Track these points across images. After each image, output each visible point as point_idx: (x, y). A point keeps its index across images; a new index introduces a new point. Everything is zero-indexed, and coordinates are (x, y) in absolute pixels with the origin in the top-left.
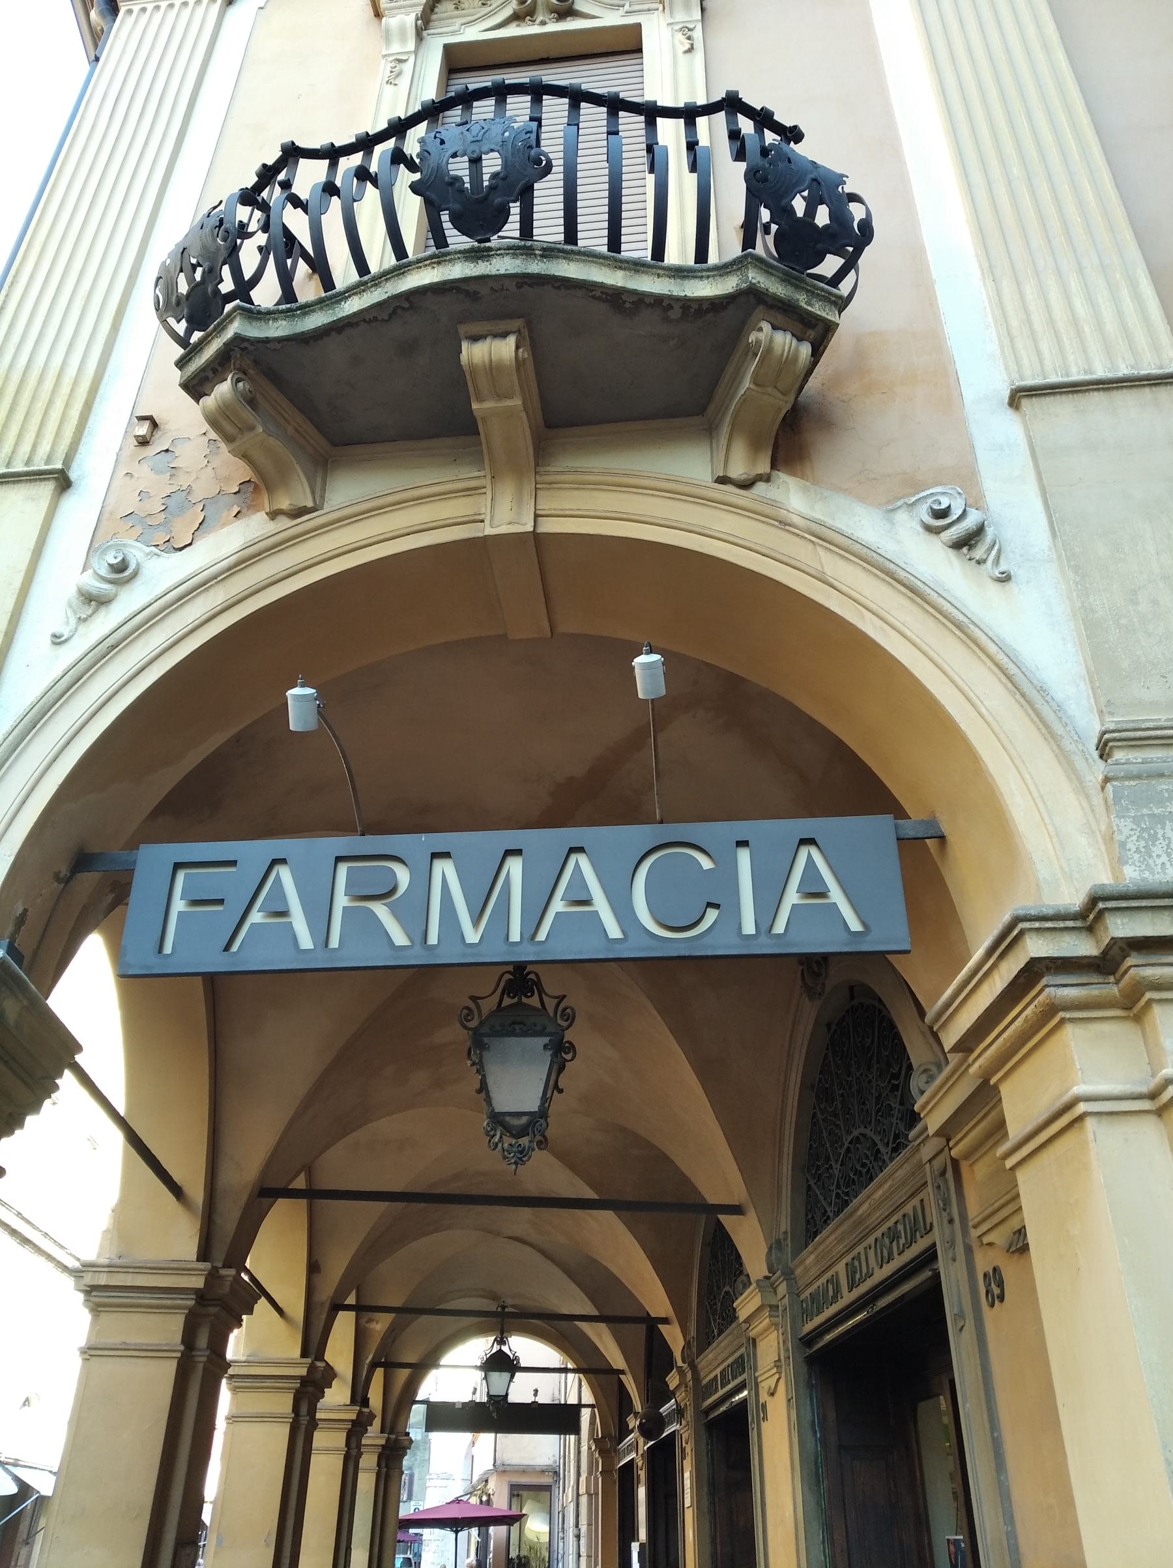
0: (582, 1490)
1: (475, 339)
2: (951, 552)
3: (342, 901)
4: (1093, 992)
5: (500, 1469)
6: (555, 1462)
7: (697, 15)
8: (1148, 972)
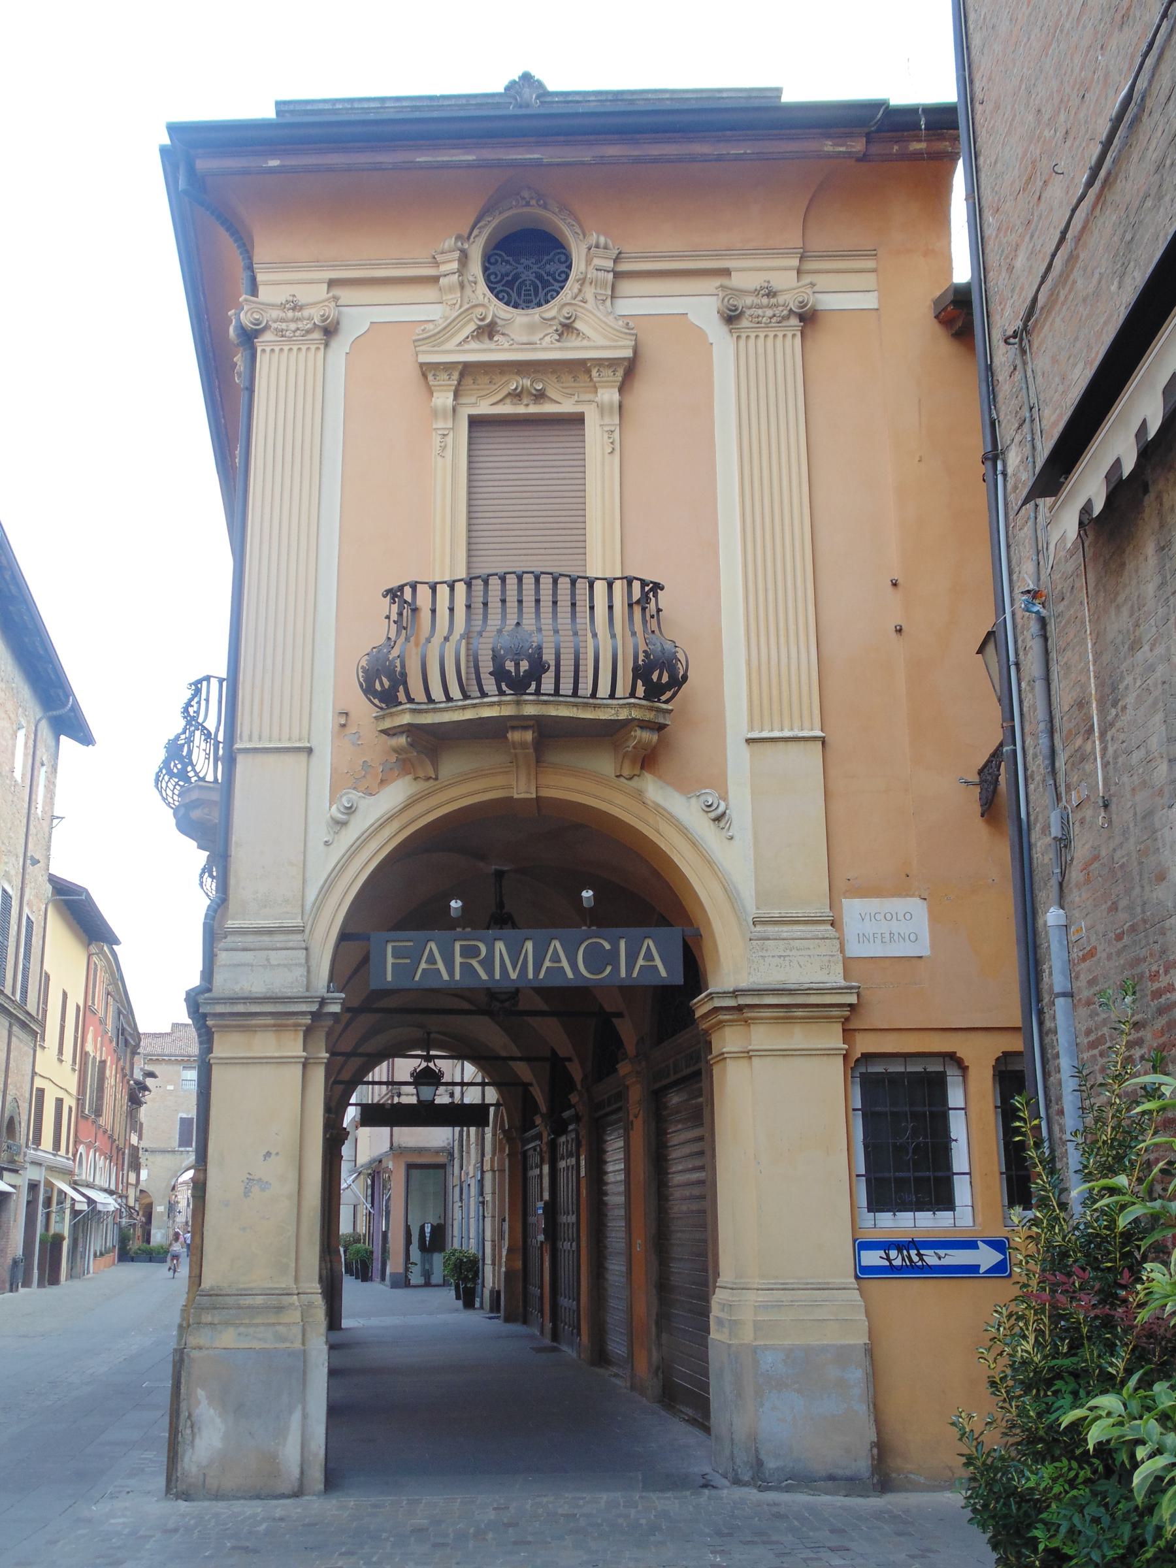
0: (487, 1167)
2: (712, 822)
3: (458, 960)
4: (735, 1017)
5: (396, 1150)
6: (449, 1144)
7: (617, 421)
8: (749, 1015)
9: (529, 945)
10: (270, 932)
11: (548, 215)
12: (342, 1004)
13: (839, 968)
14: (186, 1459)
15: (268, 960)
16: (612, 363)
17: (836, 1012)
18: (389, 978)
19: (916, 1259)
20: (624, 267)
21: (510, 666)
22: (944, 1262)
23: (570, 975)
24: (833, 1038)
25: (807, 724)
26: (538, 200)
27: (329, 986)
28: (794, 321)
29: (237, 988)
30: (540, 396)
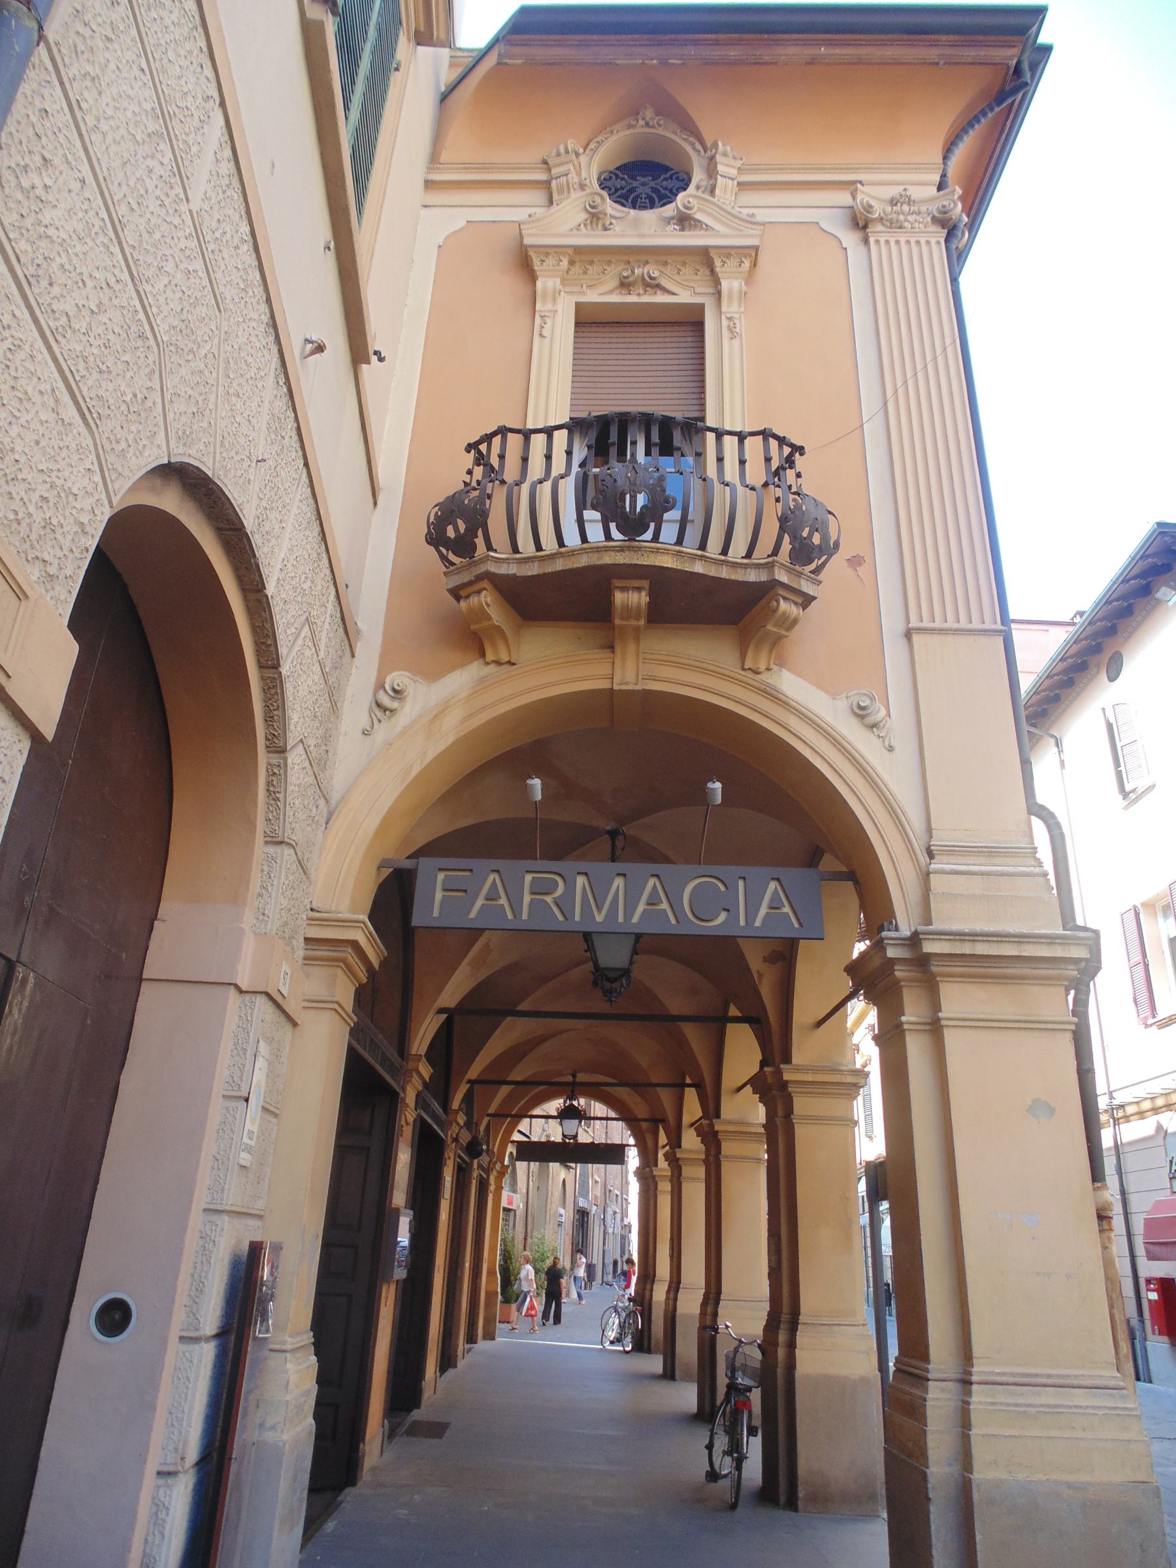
1: (623, 589)
18: (436, 914)
30: (652, 285)
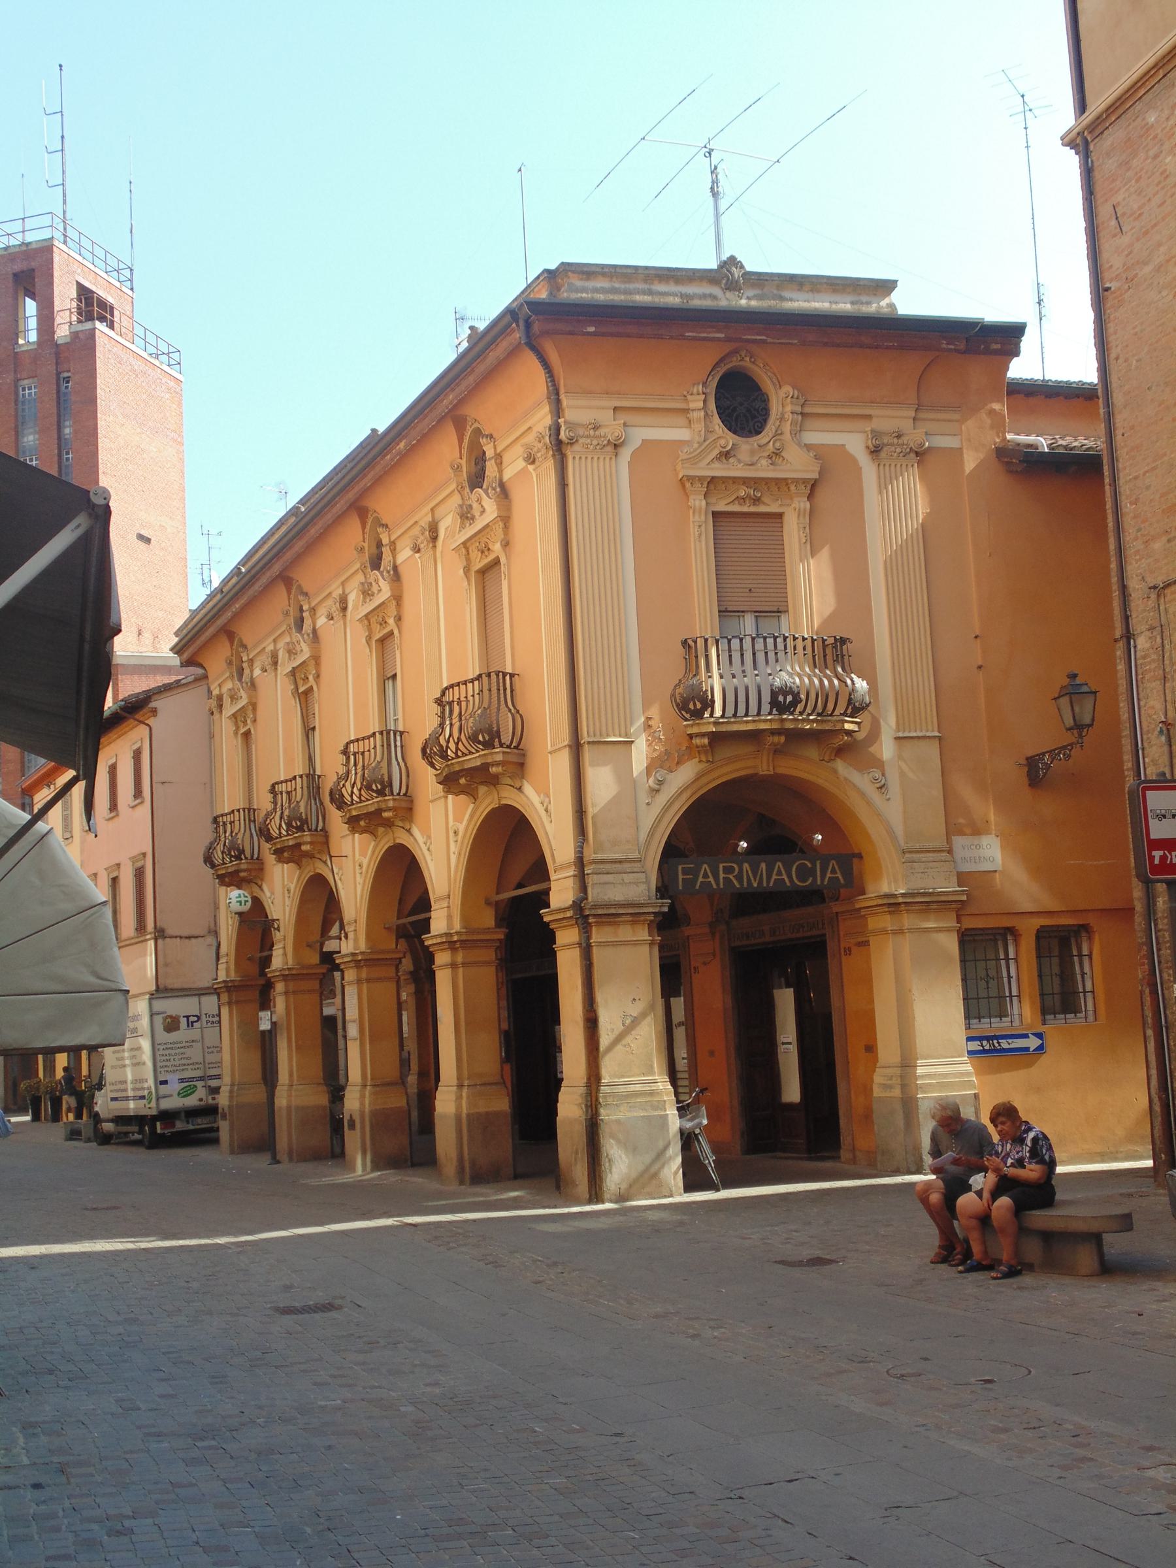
3: (722, 875)
9: (763, 865)
10: (620, 862)
11: (756, 368)
12: (669, 907)
13: (955, 879)
14: (608, 1180)
15: (623, 880)
16: (805, 481)
17: (954, 906)
18: (681, 888)
19: (997, 1045)
20: (807, 410)
21: (781, 698)
22: (1011, 1046)
23: (788, 884)
24: (952, 923)
25: (930, 728)
26: (751, 358)
27: (657, 895)
28: (913, 455)
29: (606, 898)
30: (756, 501)
